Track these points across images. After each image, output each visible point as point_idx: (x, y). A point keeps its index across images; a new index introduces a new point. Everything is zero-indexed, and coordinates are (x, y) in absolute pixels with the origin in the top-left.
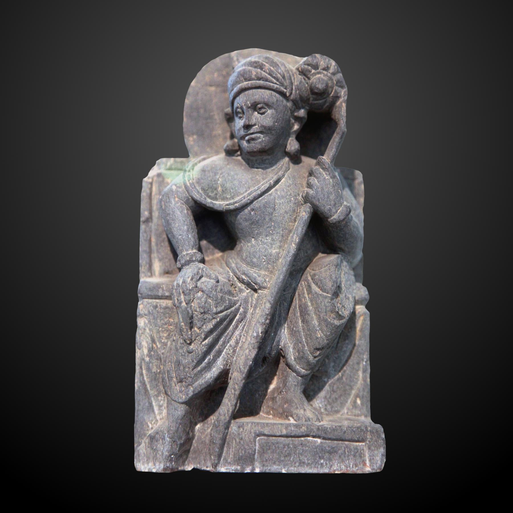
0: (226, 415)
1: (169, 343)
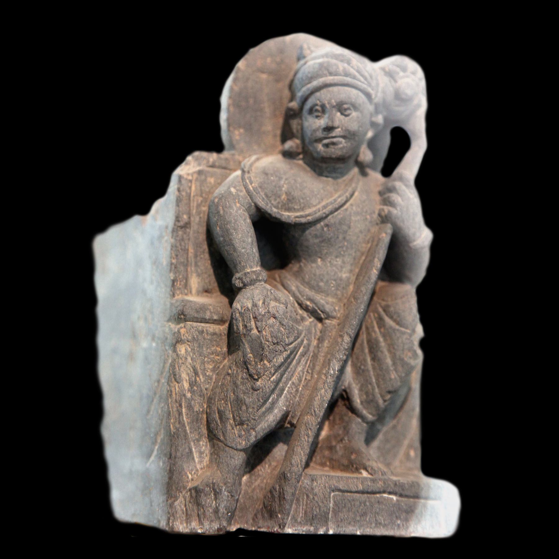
0: (299, 466)
1: (214, 376)
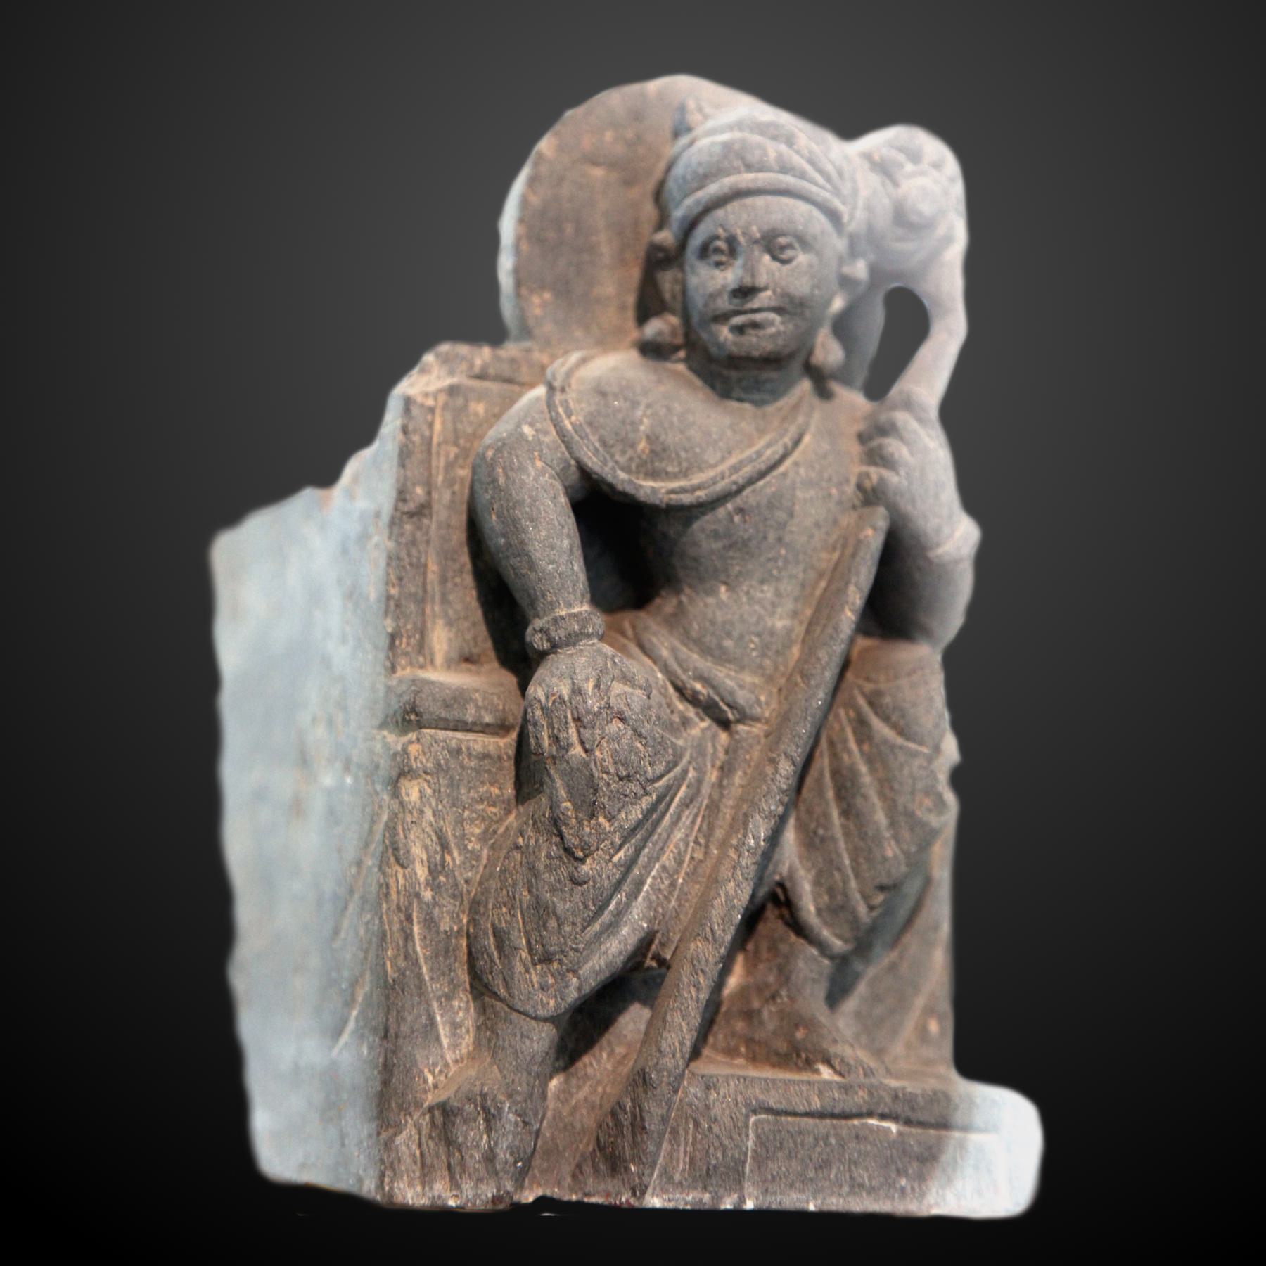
0: (678, 1055)
1: (485, 852)
